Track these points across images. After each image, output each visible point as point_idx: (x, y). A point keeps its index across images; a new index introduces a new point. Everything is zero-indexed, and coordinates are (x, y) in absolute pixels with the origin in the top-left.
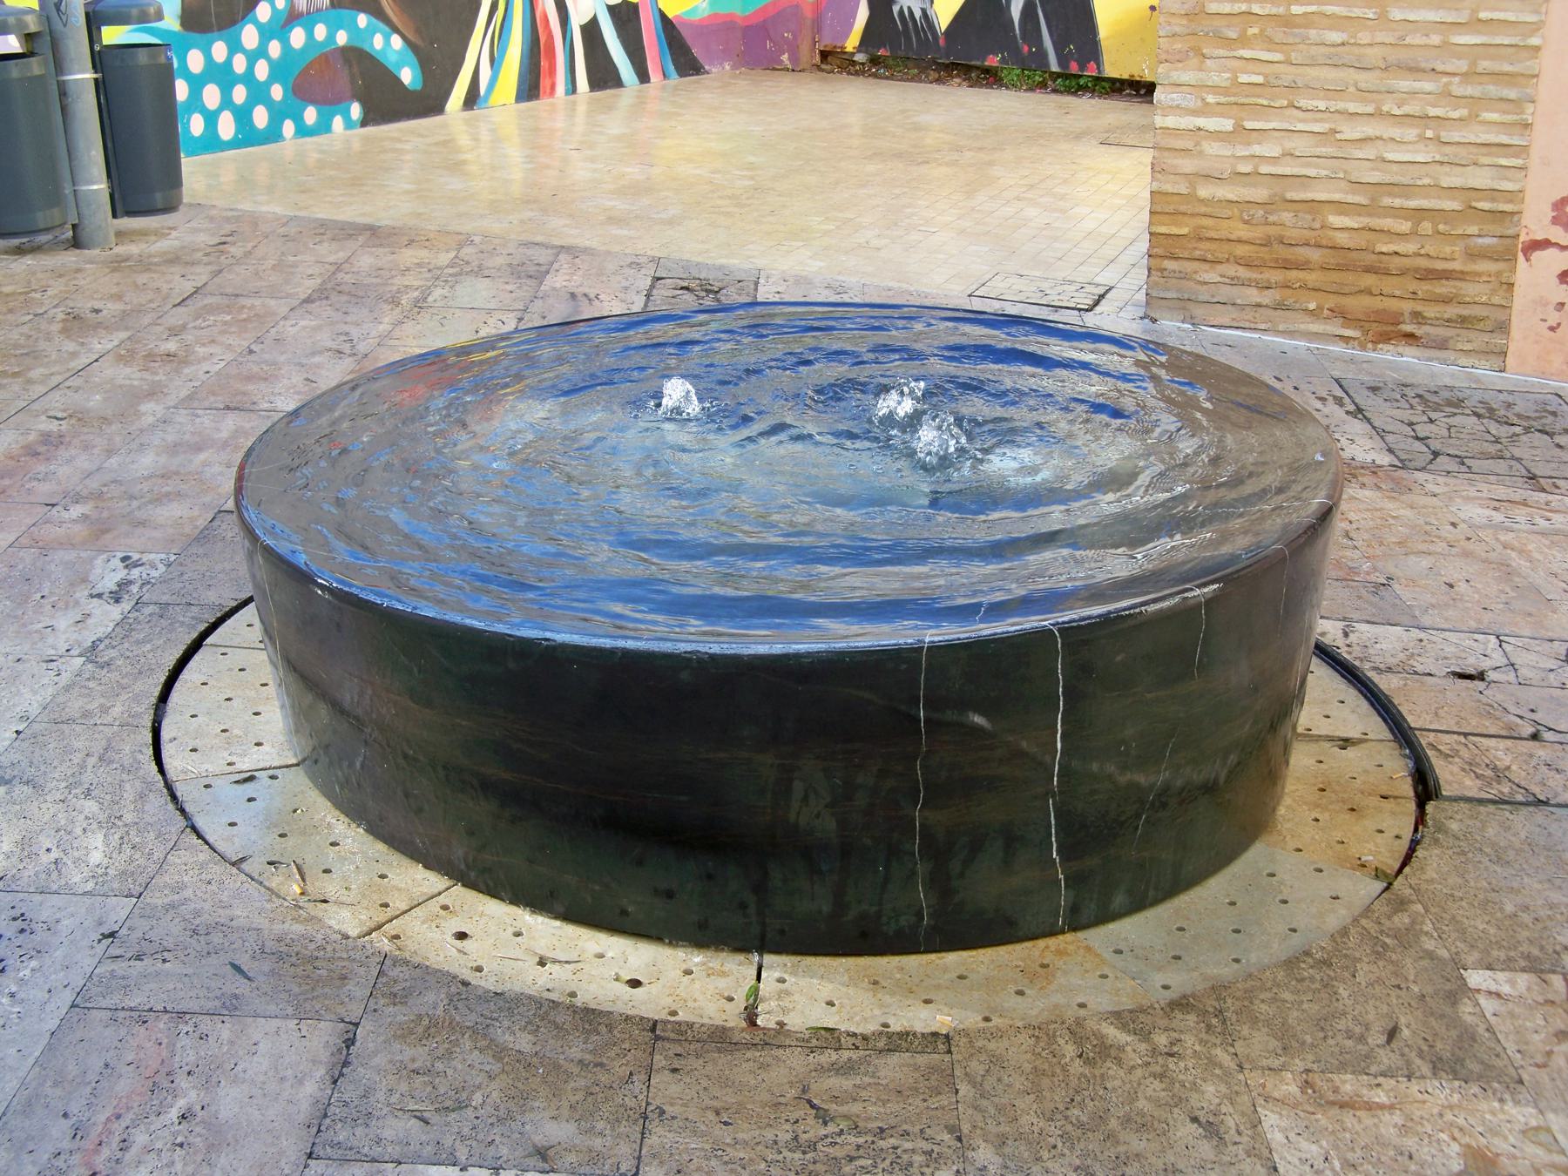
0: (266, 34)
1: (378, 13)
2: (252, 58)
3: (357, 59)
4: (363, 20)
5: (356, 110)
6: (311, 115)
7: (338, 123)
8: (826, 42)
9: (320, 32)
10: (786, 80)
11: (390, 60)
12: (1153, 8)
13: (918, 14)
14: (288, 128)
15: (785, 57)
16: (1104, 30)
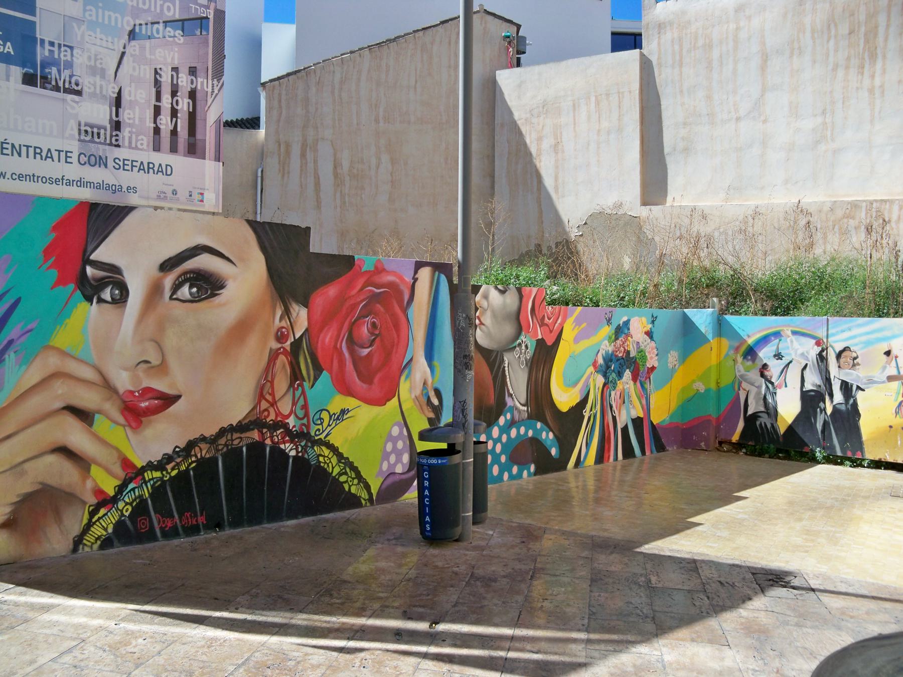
0: (502, 431)
1: (545, 422)
2: (496, 441)
3: (535, 442)
4: (539, 425)
5: (533, 468)
6: (515, 469)
7: (525, 473)
8: (722, 437)
9: (522, 430)
10: (703, 456)
11: (548, 444)
12: (891, 427)
13: (769, 426)
14: (506, 476)
15: (703, 444)
16: (864, 438)
